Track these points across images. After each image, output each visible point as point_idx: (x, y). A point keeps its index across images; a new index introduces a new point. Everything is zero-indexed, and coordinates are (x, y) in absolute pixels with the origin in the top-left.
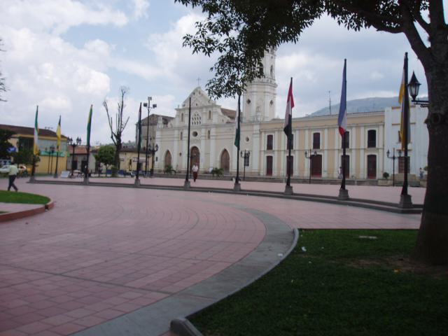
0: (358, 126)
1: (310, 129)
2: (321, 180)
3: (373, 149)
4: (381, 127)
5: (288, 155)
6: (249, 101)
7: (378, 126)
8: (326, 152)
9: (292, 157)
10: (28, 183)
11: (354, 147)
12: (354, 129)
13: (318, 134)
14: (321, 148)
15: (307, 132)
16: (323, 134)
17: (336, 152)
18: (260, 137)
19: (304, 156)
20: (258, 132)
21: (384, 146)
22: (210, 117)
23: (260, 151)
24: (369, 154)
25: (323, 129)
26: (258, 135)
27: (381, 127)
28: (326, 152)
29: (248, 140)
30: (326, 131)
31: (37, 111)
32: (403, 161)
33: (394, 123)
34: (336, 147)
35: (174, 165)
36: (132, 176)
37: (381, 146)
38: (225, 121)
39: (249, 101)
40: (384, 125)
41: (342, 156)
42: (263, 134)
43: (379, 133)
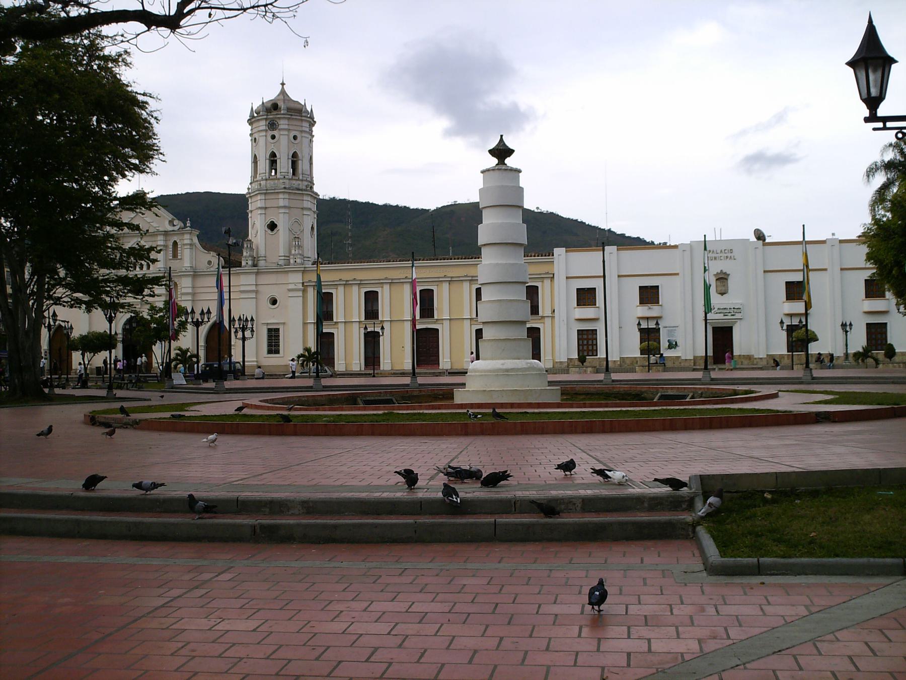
0: (347, 284)
1: (360, 284)
2: (802, 382)
4: (547, 282)
6: (272, 226)
10: (103, 478)
11: (387, 318)
12: (341, 289)
13: (375, 293)
15: (355, 288)
17: (356, 326)
18: (304, 298)
20: (300, 286)
22: (175, 256)
25: (439, 282)
26: (300, 294)
28: (446, 324)
29: (274, 302)
31: (606, 194)
33: (843, 267)
35: (362, 369)
36: (98, 421)
37: (548, 313)
39: (272, 226)
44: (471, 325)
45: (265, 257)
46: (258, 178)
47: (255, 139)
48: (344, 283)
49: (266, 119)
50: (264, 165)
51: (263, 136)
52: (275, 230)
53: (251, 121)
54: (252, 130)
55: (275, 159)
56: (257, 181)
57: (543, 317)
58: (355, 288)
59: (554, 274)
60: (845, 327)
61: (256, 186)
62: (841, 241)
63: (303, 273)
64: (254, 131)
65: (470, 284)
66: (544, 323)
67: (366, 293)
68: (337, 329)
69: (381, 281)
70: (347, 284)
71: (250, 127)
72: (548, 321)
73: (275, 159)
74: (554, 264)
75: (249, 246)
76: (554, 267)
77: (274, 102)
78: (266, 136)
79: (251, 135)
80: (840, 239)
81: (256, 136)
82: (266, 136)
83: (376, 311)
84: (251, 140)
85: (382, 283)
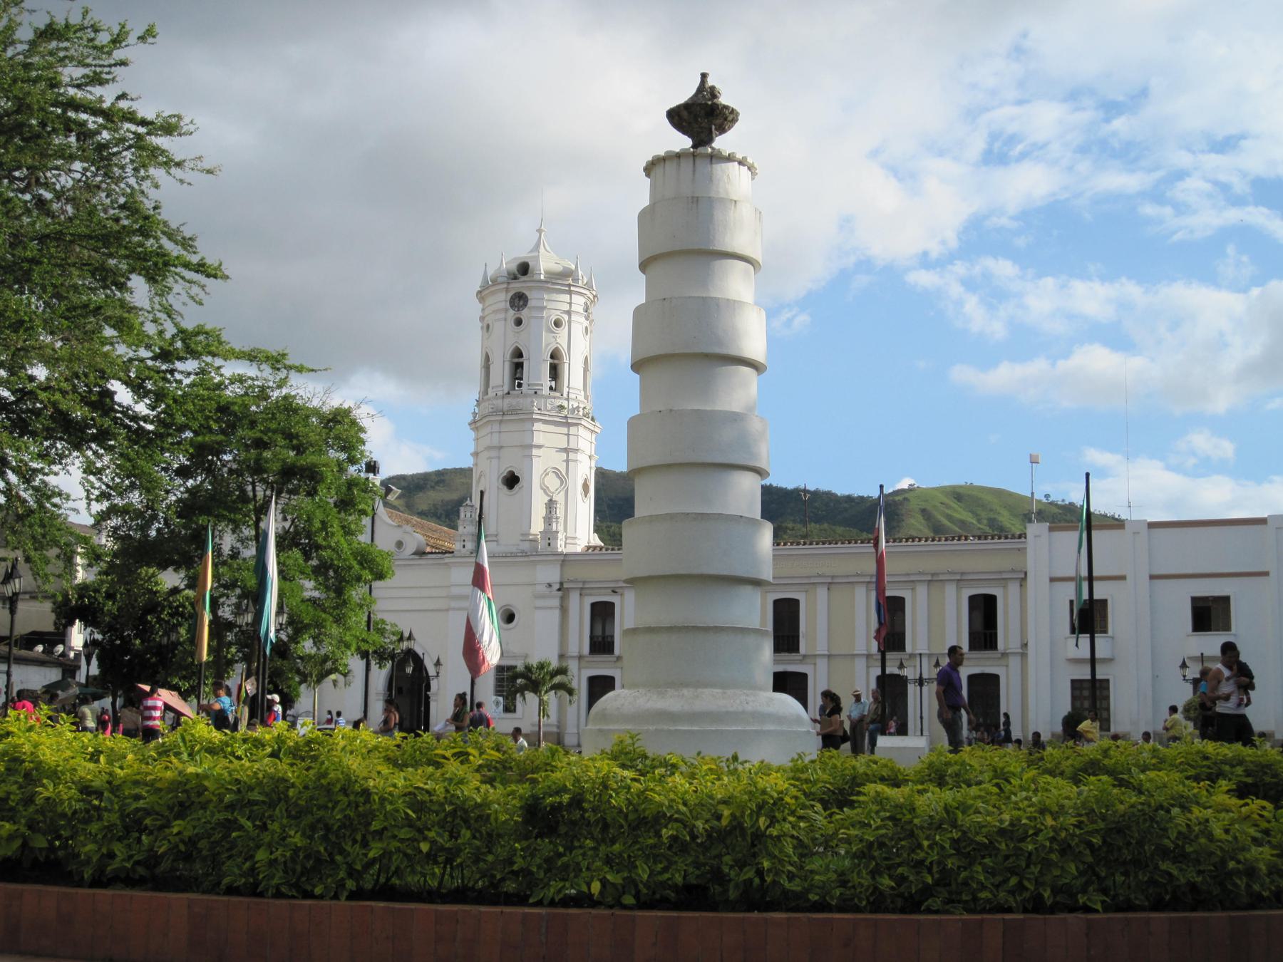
1: (960, 582)
3: (793, 656)
4: (1014, 588)
5: (878, 672)
7: (1003, 582)
8: (822, 665)
9: (1105, 683)
12: (922, 591)
13: (794, 604)
14: (803, 648)
15: (950, 590)
16: (1006, 598)
17: (860, 664)
19: (1179, 672)
21: (1025, 645)
23: (1024, 655)
24: (780, 668)
25: (810, 585)
27: (1014, 588)
28: (822, 665)
30: (822, 593)
32: (1086, 693)
33: (1157, 572)
34: (860, 648)
38: (410, 548)
40: (1024, 580)
41: (878, 678)
42: (574, 598)
43: (1006, 605)
44: (868, 667)
45: (496, 536)
46: (491, 393)
47: (488, 326)
48: (930, 578)
49: (507, 290)
50: (501, 372)
51: (499, 320)
52: (517, 487)
53: (481, 295)
54: (483, 310)
55: (521, 360)
56: (489, 400)
57: (1005, 655)
58: (950, 590)
59: (1026, 573)
60: (858, 698)
61: (487, 409)
62: (1152, 525)
63: (562, 566)
64: (486, 313)
65: (959, 589)
66: (1007, 666)
67: (594, 605)
68: (1005, 668)
69: (912, 578)
70: (934, 581)
71: (481, 306)
72: (1014, 662)
73: (521, 360)
74: (1026, 553)
75: (468, 515)
76: (1026, 557)
77: (523, 260)
78: (505, 320)
79: (482, 319)
80: (1150, 520)
81: (488, 320)
82: (505, 320)
83: (609, 639)
84: (482, 328)
85: (814, 584)
